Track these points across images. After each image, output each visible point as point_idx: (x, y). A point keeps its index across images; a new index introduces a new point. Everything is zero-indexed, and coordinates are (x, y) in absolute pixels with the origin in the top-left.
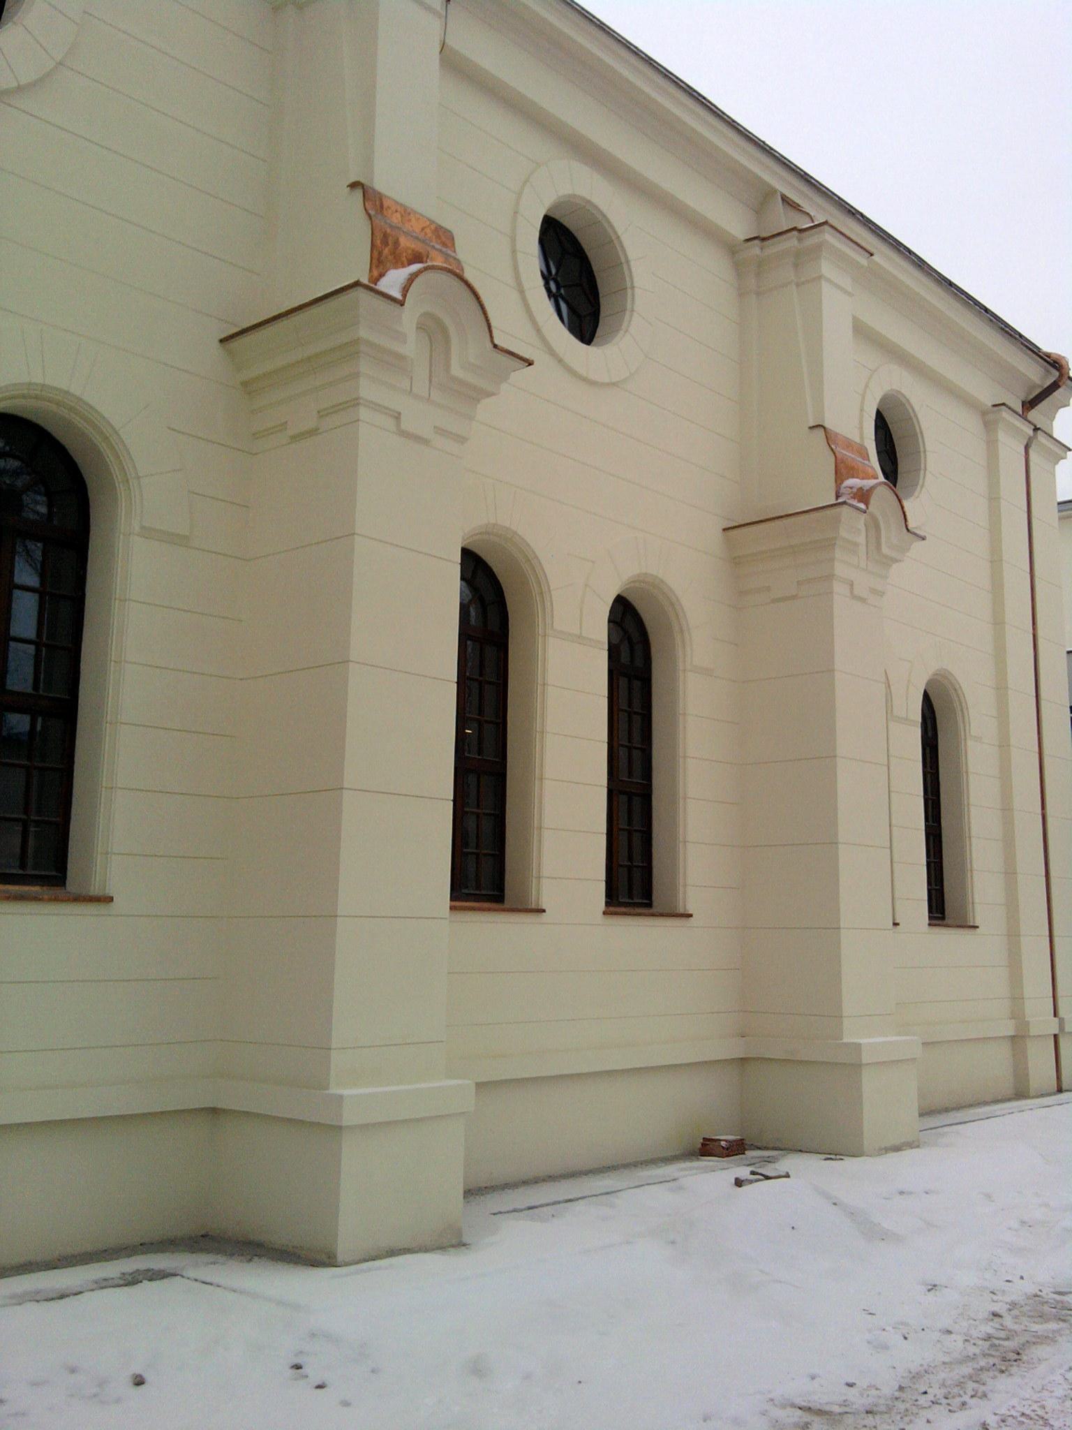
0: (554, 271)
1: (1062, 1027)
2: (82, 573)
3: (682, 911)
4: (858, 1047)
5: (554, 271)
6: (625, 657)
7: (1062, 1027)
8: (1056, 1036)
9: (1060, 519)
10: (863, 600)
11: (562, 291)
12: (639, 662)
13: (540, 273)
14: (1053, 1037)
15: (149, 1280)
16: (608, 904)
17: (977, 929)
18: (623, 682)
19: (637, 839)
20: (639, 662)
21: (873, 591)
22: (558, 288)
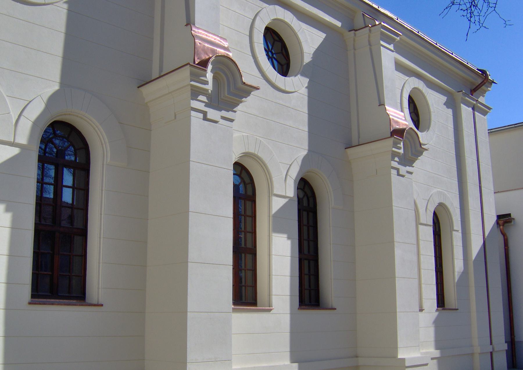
0: (270, 47)
1: (493, 349)
2: (87, 188)
3: (95, 302)
4: (403, 360)
5: (270, 47)
6: (305, 203)
7: (493, 349)
8: (491, 353)
9: (488, 133)
10: (403, 176)
11: (274, 56)
12: (311, 205)
13: (264, 48)
14: (490, 353)
15: (435, 208)
16: (33, 296)
17: (458, 310)
18: (305, 214)
19: (311, 243)
20: (311, 205)
21: (408, 172)
22: (272, 54)
